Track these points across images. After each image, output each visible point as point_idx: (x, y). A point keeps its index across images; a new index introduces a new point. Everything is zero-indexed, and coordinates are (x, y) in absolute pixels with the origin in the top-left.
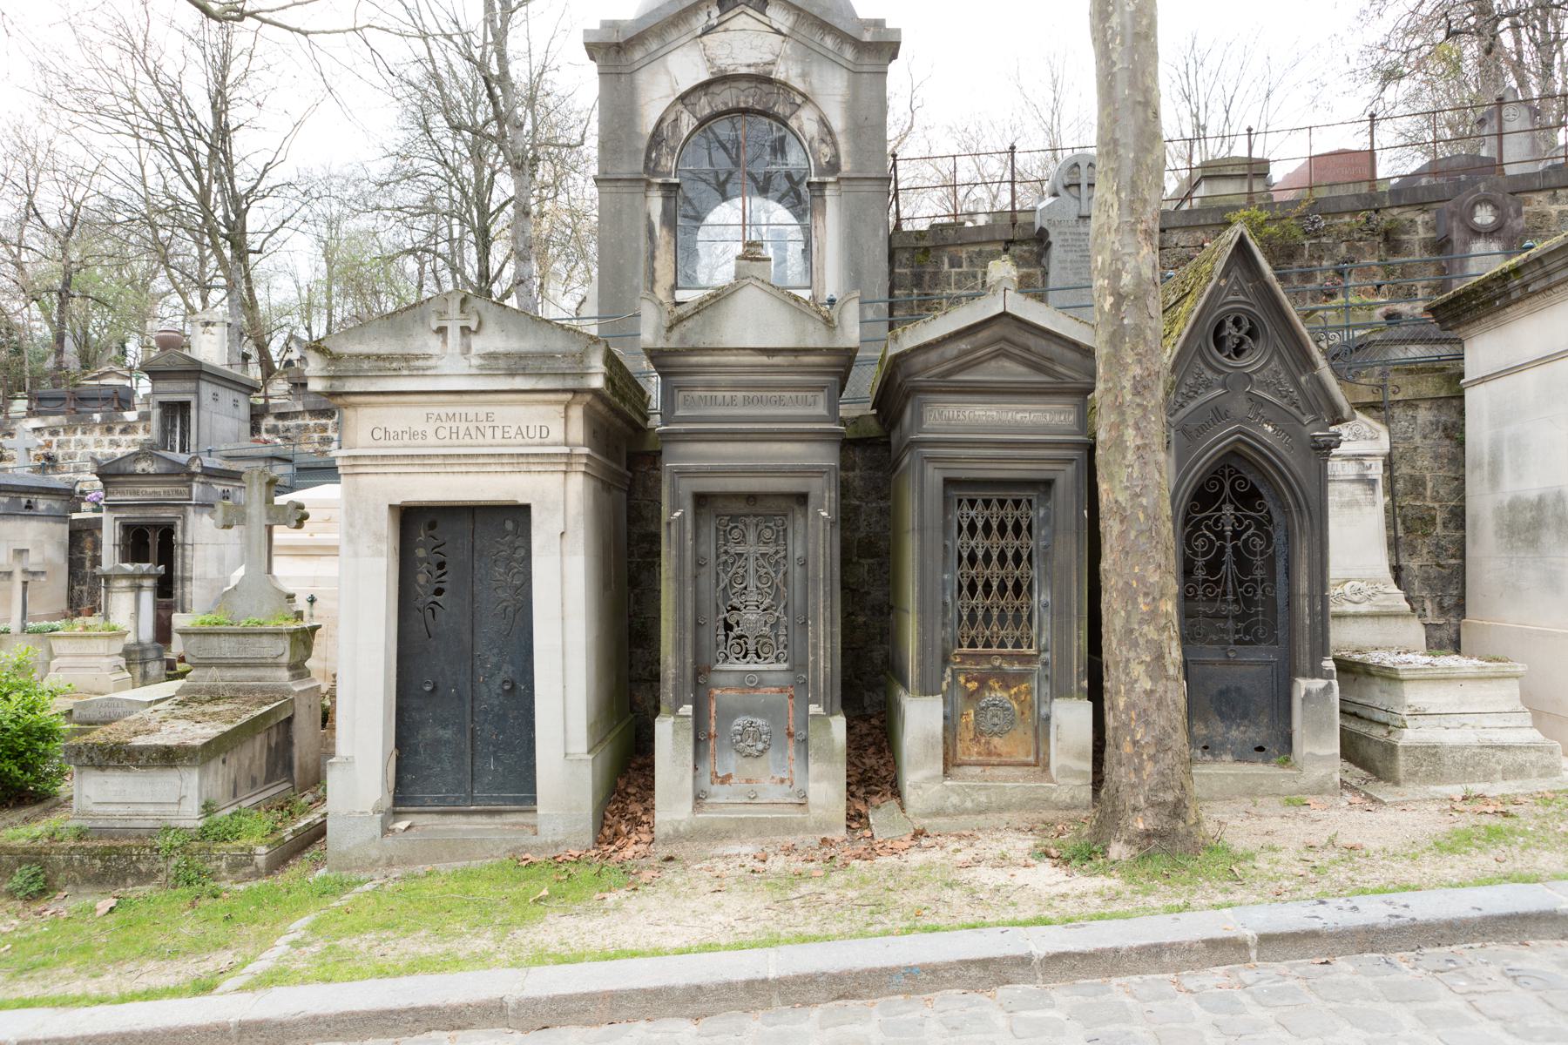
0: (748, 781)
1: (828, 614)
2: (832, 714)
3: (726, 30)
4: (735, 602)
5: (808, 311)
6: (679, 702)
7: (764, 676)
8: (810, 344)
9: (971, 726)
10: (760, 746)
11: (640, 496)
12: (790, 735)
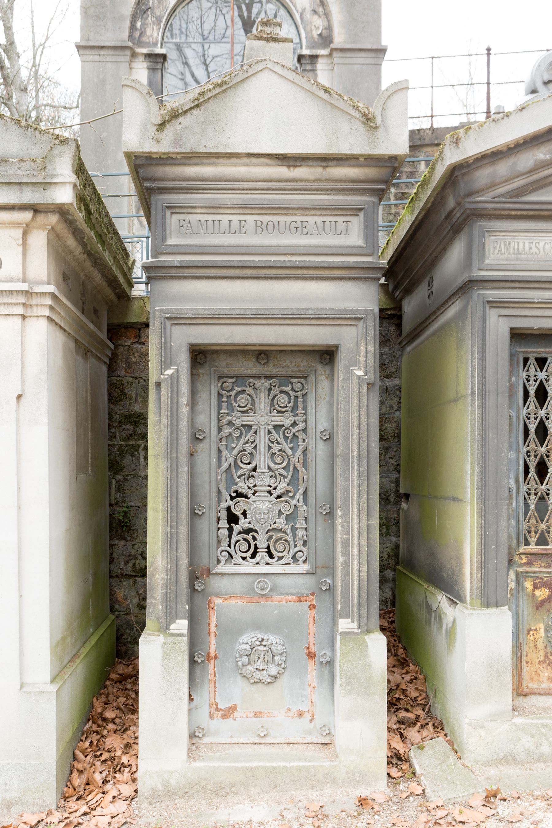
0: (257, 714)
1: (364, 502)
2: (368, 632)
3: (204, 22)
4: (242, 486)
5: (341, 105)
6: (170, 616)
7: (281, 581)
8: (344, 147)
9: (540, 645)
10: (273, 670)
11: (123, 373)
12: (311, 655)
